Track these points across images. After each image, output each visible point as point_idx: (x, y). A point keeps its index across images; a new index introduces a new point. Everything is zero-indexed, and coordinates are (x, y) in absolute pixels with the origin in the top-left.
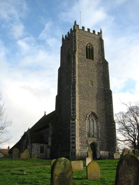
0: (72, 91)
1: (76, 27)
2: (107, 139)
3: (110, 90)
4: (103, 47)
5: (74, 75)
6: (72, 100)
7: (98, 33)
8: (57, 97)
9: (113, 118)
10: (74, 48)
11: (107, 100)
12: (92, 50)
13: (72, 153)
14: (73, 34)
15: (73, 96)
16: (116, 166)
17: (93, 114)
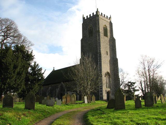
0: (98, 58)
1: (98, 13)
2: (115, 89)
3: (117, 58)
4: (112, 28)
5: (99, 47)
6: (99, 64)
7: (109, 18)
8: (83, 24)
9: (119, 76)
10: (97, 28)
11: (115, 65)
12: (107, 29)
13: (100, 97)
14: (97, 18)
15: (99, 61)
16: (43, 73)
17: (108, 73)
